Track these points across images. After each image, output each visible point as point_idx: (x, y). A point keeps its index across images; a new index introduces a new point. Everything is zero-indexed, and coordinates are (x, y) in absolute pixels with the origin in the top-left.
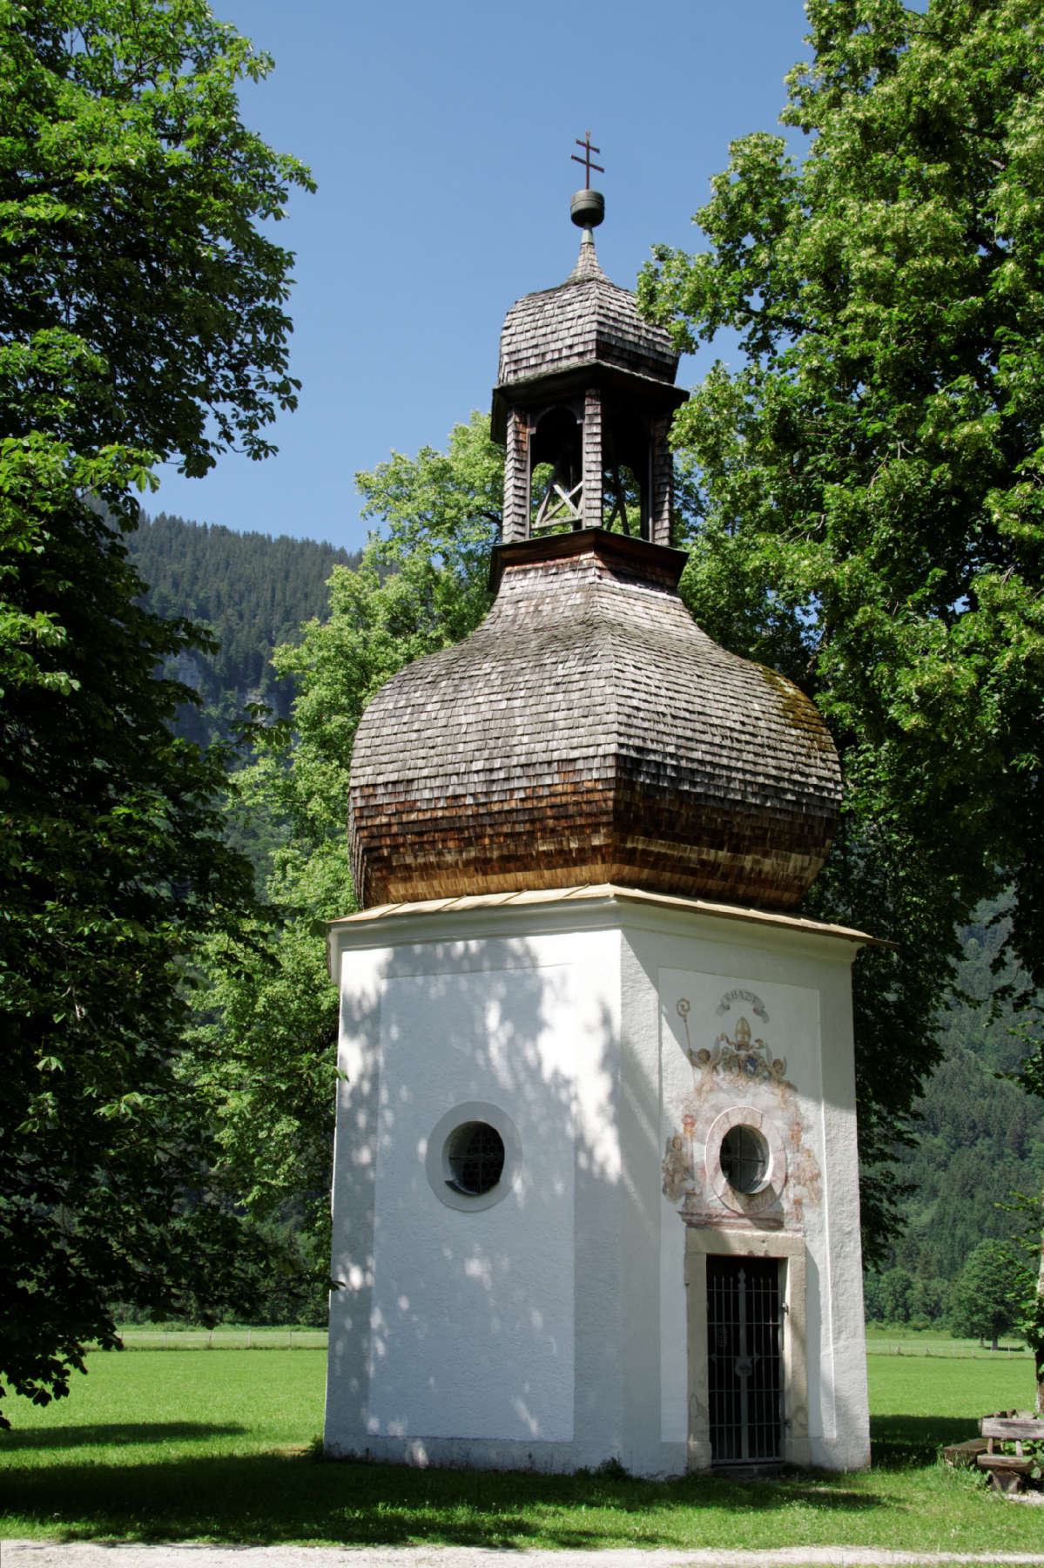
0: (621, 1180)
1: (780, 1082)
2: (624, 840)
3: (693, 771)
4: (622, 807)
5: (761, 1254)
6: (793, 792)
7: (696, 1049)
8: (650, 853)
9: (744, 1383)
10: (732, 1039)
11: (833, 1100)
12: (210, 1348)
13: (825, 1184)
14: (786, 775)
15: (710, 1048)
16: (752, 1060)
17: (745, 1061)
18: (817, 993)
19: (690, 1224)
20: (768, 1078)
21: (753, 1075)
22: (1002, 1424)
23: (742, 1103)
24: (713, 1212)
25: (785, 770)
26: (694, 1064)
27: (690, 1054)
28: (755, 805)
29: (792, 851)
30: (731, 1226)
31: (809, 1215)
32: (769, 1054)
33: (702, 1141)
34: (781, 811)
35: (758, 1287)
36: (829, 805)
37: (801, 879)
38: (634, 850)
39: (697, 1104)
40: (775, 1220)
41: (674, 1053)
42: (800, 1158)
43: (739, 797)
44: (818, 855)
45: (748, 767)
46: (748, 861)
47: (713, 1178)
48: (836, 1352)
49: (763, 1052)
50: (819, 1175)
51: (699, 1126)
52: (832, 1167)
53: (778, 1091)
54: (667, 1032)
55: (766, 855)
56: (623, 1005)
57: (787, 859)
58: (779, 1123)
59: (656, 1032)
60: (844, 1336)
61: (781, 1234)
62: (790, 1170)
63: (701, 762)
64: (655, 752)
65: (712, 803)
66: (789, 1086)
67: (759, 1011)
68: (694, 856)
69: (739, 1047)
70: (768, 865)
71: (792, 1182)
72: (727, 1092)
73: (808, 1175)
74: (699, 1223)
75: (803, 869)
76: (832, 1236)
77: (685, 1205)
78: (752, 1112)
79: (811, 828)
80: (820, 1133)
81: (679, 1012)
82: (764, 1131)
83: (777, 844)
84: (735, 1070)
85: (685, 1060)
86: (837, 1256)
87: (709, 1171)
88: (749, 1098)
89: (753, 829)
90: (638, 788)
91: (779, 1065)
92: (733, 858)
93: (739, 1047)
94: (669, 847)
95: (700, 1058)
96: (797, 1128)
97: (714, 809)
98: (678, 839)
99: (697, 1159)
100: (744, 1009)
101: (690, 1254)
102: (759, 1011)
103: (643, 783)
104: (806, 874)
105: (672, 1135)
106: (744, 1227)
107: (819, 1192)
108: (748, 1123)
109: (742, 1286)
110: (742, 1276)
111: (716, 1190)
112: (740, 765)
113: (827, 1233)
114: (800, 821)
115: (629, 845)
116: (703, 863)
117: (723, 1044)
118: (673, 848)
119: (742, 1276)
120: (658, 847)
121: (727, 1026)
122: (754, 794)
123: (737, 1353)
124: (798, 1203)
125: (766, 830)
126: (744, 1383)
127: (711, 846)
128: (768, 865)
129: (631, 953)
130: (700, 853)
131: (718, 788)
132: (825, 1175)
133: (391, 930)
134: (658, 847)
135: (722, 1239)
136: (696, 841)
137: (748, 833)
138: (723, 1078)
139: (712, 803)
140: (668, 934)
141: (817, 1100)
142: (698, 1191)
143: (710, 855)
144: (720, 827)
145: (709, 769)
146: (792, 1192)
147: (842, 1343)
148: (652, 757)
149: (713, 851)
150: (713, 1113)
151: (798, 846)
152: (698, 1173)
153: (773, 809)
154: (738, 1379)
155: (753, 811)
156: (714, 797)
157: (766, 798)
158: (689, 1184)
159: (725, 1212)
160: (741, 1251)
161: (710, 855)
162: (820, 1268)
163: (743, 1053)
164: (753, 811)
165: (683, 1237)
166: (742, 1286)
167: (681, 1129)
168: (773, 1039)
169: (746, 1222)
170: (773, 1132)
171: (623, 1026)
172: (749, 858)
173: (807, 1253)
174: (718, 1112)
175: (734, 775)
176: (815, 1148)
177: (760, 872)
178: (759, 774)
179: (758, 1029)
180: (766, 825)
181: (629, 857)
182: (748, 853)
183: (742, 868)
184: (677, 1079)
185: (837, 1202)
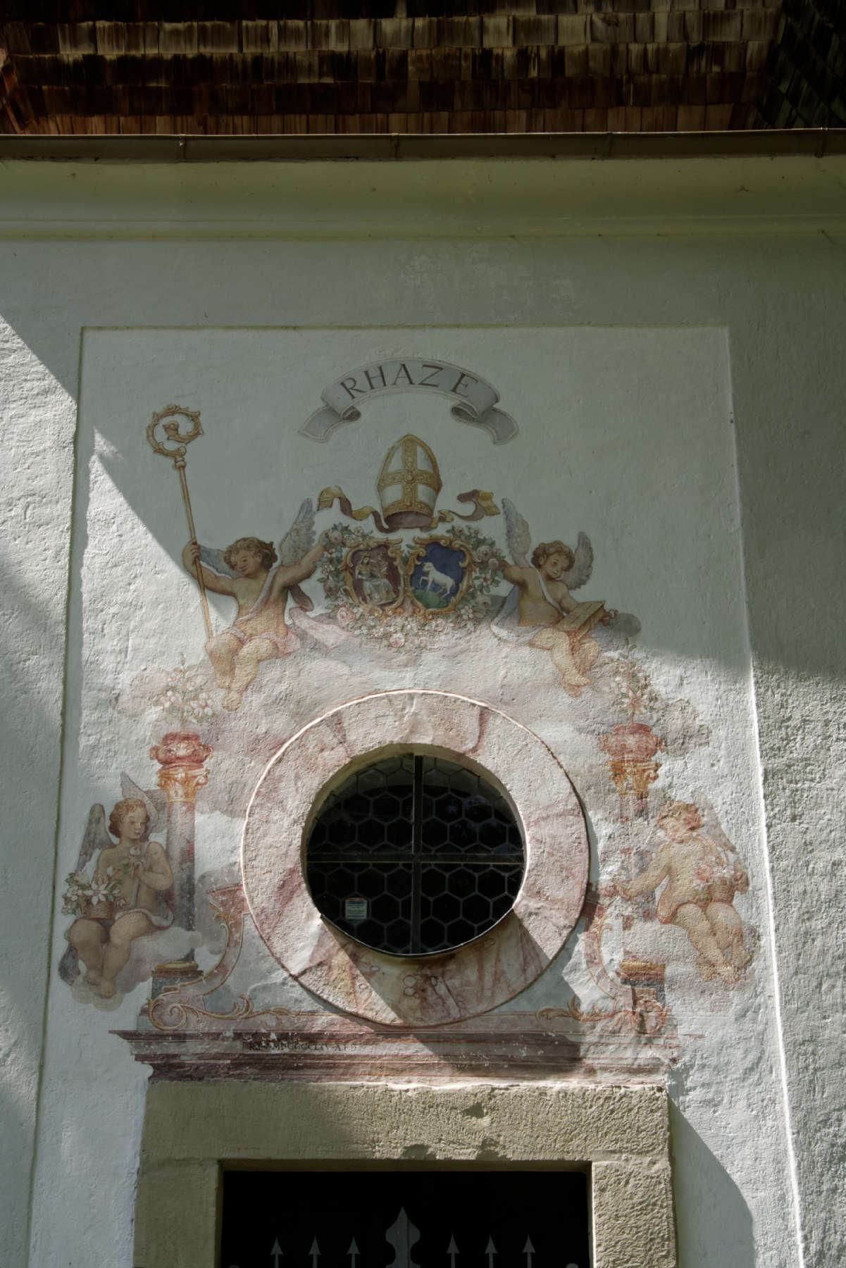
1: (559, 615)
2: (47, 42)
5: (467, 1154)
7: (218, 539)
10: (365, 497)
11: (779, 654)
15: (272, 534)
17: (423, 564)
19: (166, 1069)
20: (514, 608)
26: (205, 585)
27: (196, 562)
31: (695, 1018)
33: (231, 807)
37: (717, 53)
39: (217, 699)
40: (537, 1039)
49: (492, 528)
50: (738, 884)
54: (106, 498)
58: (558, 733)
61: (574, 1083)
62: (607, 874)
66: (604, 621)
67: (481, 411)
68: (298, 50)
69: (392, 521)
71: (611, 914)
72: (339, 653)
73: (688, 883)
77: (152, 1009)
78: (445, 710)
80: (738, 751)
81: (164, 451)
82: (490, 760)
93: (392, 521)
94: (204, 37)
95: (241, 571)
96: (634, 752)
101: (155, 1170)
104: (729, 34)
105: (112, 792)
106: (424, 1068)
107: (743, 943)
108: (425, 738)
115: (70, 54)
116: (341, 65)
124: (644, 979)
130: (316, 37)
141: (726, 660)
146: (616, 942)
149: (360, 25)
159: (323, 1022)
162: (753, 1199)
163: (406, 538)
168: (529, 487)
169: (414, 1049)
172: (498, 21)
173: (677, 1137)
176: (720, 799)
177: (557, 58)
179: (466, 459)
183: (486, 58)
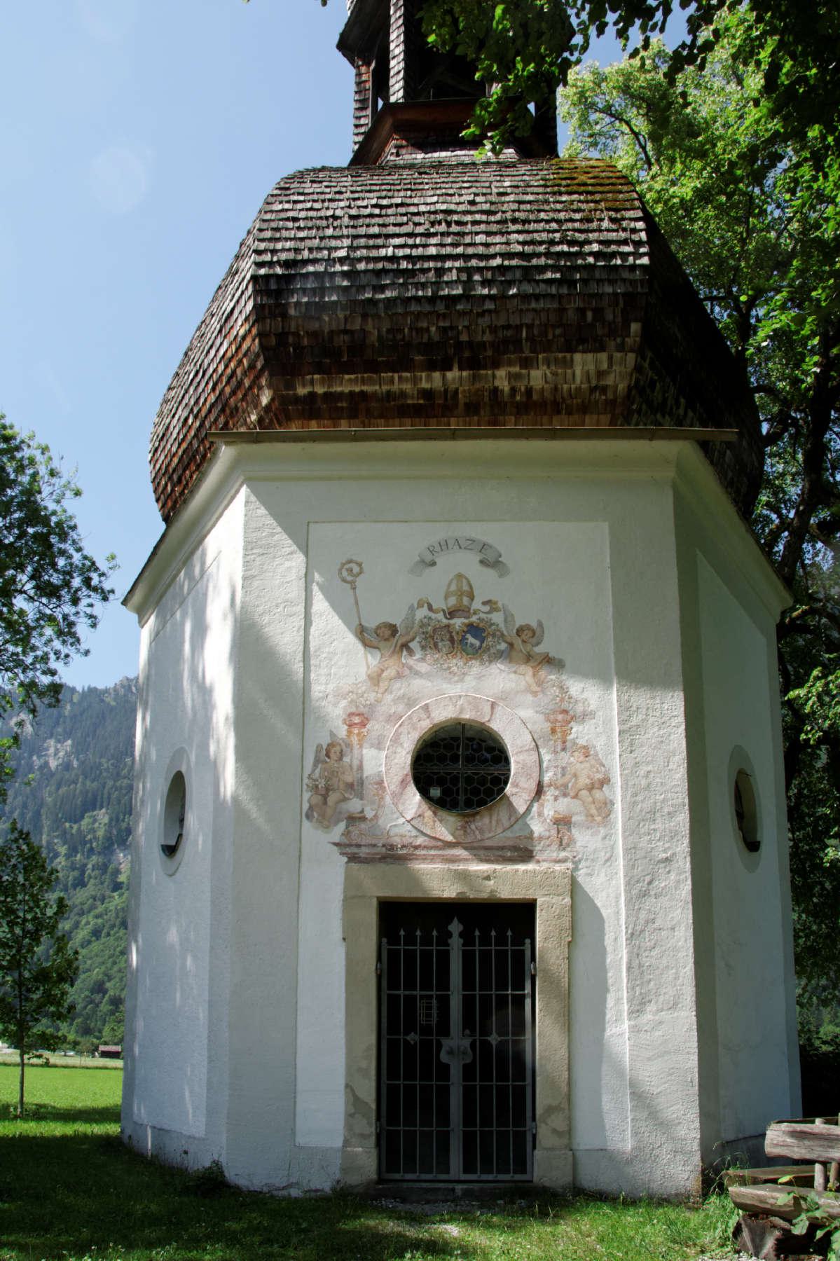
0: (235, 799)
1: (528, 658)
3: (379, 273)
4: (273, 341)
6: (555, 268)
7: (371, 624)
8: (340, 396)
9: (456, 1074)
10: (439, 604)
11: (632, 672)
12: (106, 1068)
13: (617, 793)
14: (542, 249)
15: (397, 621)
16: (475, 630)
18: (605, 526)
19: (353, 858)
20: (508, 655)
21: (475, 653)
22: (793, 1134)
23: (455, 689)
24: (397, 841)
25: (541, 243)
26: (366, 644)
27: (362, 633)
28: (489, 297)
29: (572, 350)
30: (424, 859)
31: (584, 839)
32: (508, 618)
33: (379, 746)
34: (537, 297)
35: (485, 940)
36: (626, 275)
37: (604, 389)
38: (312, 395)
39: (372, 697)
40: (515, 848)
41: (331, 630)
42: (571, 759)
43: (458, 291)
44: (621, 348)
45: (481, 250)
46: (501, 379)
47: (398, 796)
48: (635, 1030)
49: (497, 618)
50: (605, 781)
51: (374, 727)
52: (629, 772)
53: (527, 670)
54: (320, 604)
55: (527, 363)
56: (245, 579)
57: (570, 364)
58: (527, 713)
59: (301, 608)
60: (651, 1007)
61: (530, 867)
63: (393, 259)
64: (315, 261)
65: (414, 307)
66: (549, 661)
67: (493, 562)
68: (407, 387)
69: (451, 614)
70: (538, 377)
72: (427, 676)
73: (584, 781)
74: (372, 854)
75: (601, 374)
76: (631, 866)
77: (347, 833)
78: (475, 703)
79: (598, 312)
80: (607, 722)
83: (541, 344)
84: (444, 645)
85: (351, 639)
86: (640, 891)
87: (392, 784)
88: (470, 681)
89: (493, 329)
90: (292, 312)
91: (529, 634)
92: (474, 378)
93: (451, 614)
95: (383, 637)
96: (562, 720)
97: (418, 316)
98: (373, 367)
99: (369, 770)
100: (468, 564)
101: (351, 899)
102: (493, 562)
103: (298, 304)
104: (609, 381)
105: (325, 741)
107: (606, 808)
109: (456, 944)
110: (455, 927)
111: (406, 812)
112: (460, 250)
113: (621, 861)
114: (579, 303)
115: (302, 391)
116: (428, 394)
117: (422, 613)
118: (370, 382)
119: (455, 927)
120: (346, 385)
121: (435, 588)
122: (484, 283)
123: (444, 1030)
124: (562, 822)
125: (518, 328)
126: (456, 1074)
127: (431, 366)
128: (538, 377)
129: (263, 511)
130: (416, 381)
131: (423, 286)
132: (617, 780)
133: (152, 589)
134: (346, 385)
135: (414, 879)
136: (402, 364)
137: (488, 337)
138: (420, 662)
139: (414, 307)
140: (329, 479)
141: (605, 681)
142: (369, 814)
143: (434, 381)
144: (436, 338)
145: (404, 265)
146: (551, 807)
147: (648, 1017)
148: (311, 269)
150: (401, 708)
151: (582, 341)
152: (370, 789)
153: (522, 297)
154: (444, 1070)
155: (489, 305)
156: (417, 299)
157: (510, 284)
158: (354, 805)
159: (420, 841)
160: (448, 891)
161: (434, 381)
163: (458, 622)
164: (489, 305)
165: (341, 879)
166: (456, 944)
167: (342, 731)
168: (513, 599)
170: (516, 729)
171: (243, 602)
172: (501, 373)
173: (574, 888)
174: (410, 705)
175: (448, 264)
176: (599, 744)
177: (529, 391)
178: (494, 256)
180: (515, 320)
181: (311, 408)
182: (496, 365)
183: (495, 391)
184: (338, 667)
185: (639, 820)
